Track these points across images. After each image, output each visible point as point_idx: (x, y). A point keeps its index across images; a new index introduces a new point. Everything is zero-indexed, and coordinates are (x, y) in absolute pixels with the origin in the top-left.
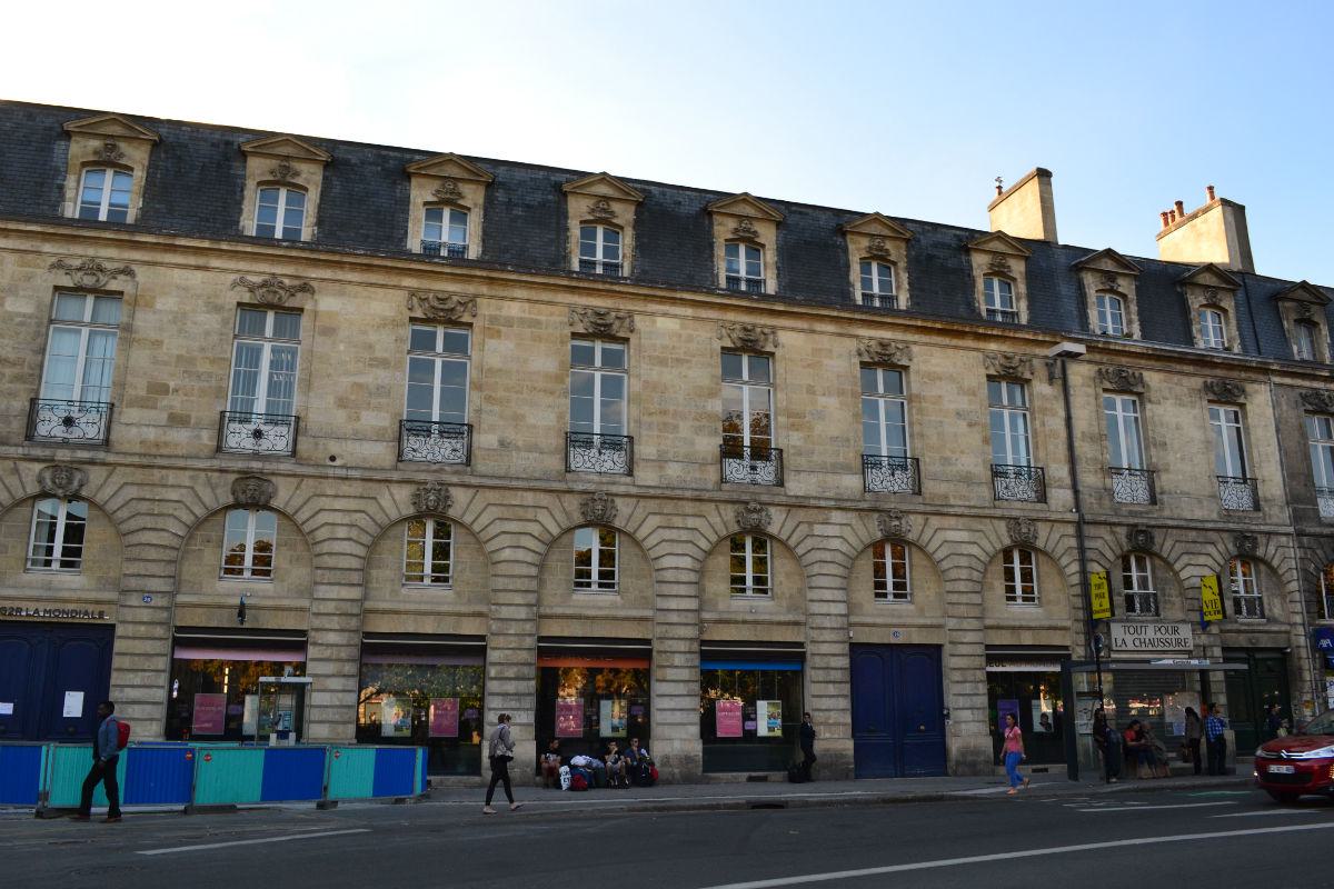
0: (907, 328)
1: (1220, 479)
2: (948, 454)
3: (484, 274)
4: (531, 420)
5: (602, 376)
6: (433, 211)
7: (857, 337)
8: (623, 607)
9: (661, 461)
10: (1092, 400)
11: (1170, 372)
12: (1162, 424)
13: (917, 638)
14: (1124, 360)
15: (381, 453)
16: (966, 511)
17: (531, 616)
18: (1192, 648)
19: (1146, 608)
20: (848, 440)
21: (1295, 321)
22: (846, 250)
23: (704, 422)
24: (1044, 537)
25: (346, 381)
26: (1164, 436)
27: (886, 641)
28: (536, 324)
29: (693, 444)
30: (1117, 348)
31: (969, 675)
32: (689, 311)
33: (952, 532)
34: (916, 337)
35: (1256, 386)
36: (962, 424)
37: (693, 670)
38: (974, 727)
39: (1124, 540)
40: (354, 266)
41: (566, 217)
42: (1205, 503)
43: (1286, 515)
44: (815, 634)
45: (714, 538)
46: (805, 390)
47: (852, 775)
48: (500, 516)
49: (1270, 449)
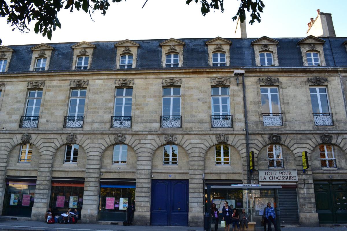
0: (180, 73)
1: (314, 114)
2: (194, 113)
3: (46, 74)
4: (56, 114)
6: (123, 56)
7: (161, 78)
8: (78, 168)
9: (93, 122)
10: (256, 90)
11: (291, 76)
12: (287, 96)
13: (178, 177)
14: (270, 74)
15: (15, 126)
16: (198, 133)
17: (49, 171)
18: (297, 180)
19: (279, 165)
20: (156, 112)
22: (161, 52)
23: (108, 110)
24: (231, 140)
25: (9, 107)
26: (288, 100)
27: (166, 178)
28: (60, 86)
29: (103, 117)
30: (265, 70)
31: (197, 191)
32: (106, 77)
33: (193, 140)
34: (184, 76)
35: (333, 78)
36: (201, 103)
37: (96, 188)
38: (198, 209)
39: (267, 140)
40: (15, 77)
41: (73, 55)
42: (306, 124)
44: (138, 176)
45: (106, 146)
46: (142, 97)
47: (148, 224)
48: (44, 142)
49: (339, 101)
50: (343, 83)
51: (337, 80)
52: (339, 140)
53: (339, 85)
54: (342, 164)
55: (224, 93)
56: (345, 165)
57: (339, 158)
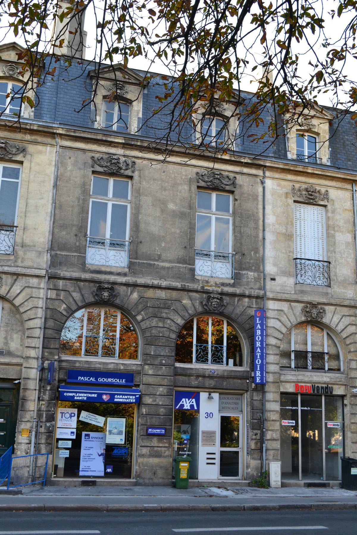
5: (113, 205)
21: (105, 97)
35: (40, 148)
43: (45, 259)
50: (61, 163)
51: (48, 154)
52: (16, 289)
53: (50, 164)
54: (12, 343)
55: (120, 193)
56: (19, 346)
57: (9, 328)
